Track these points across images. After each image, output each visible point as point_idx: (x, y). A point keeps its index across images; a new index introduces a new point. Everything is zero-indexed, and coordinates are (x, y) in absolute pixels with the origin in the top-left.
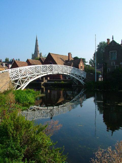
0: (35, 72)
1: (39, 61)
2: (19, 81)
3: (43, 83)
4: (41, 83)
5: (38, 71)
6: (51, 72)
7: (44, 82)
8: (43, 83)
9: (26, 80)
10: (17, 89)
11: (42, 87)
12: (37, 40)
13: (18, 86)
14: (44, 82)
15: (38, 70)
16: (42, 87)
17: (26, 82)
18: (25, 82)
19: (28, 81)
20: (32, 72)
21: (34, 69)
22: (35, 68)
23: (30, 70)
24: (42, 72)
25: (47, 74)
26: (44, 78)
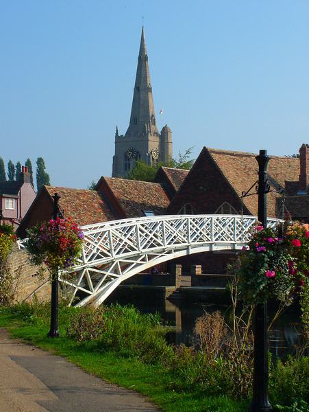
0: (87, 256)
1: (157, 185)
2: (85, 278)
3: (173, 288)
4: (163, 291)
5: (151, 239)
6: (202, 245)
7: (179, 284)
8: (173, 288)
9: (108, 273)
10: (77, 306)
11: (170, 307)
12: (142, 59)
13: (82, 295)
14: (179, 284)
15: (151, 235)
16: (170, 307)
17: (109, 279)
18: (105, 282)
19: (115, 278)
20: (129, 242)
21: (139, 232)
22: (141, 227)
23: (123, 238)
24: (166, 246)
25: (188, 252)
26: (179, 269)
